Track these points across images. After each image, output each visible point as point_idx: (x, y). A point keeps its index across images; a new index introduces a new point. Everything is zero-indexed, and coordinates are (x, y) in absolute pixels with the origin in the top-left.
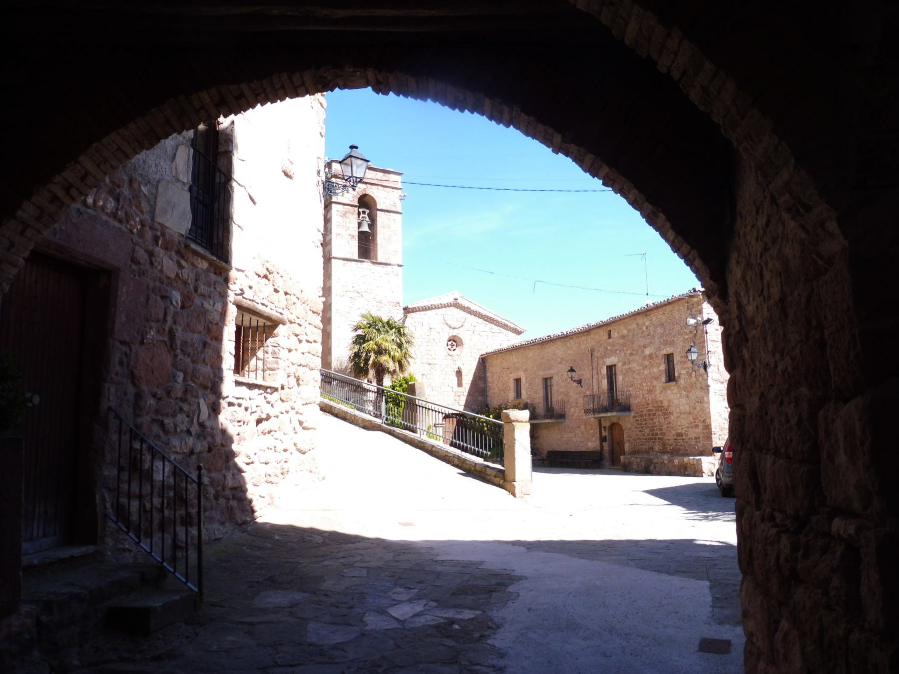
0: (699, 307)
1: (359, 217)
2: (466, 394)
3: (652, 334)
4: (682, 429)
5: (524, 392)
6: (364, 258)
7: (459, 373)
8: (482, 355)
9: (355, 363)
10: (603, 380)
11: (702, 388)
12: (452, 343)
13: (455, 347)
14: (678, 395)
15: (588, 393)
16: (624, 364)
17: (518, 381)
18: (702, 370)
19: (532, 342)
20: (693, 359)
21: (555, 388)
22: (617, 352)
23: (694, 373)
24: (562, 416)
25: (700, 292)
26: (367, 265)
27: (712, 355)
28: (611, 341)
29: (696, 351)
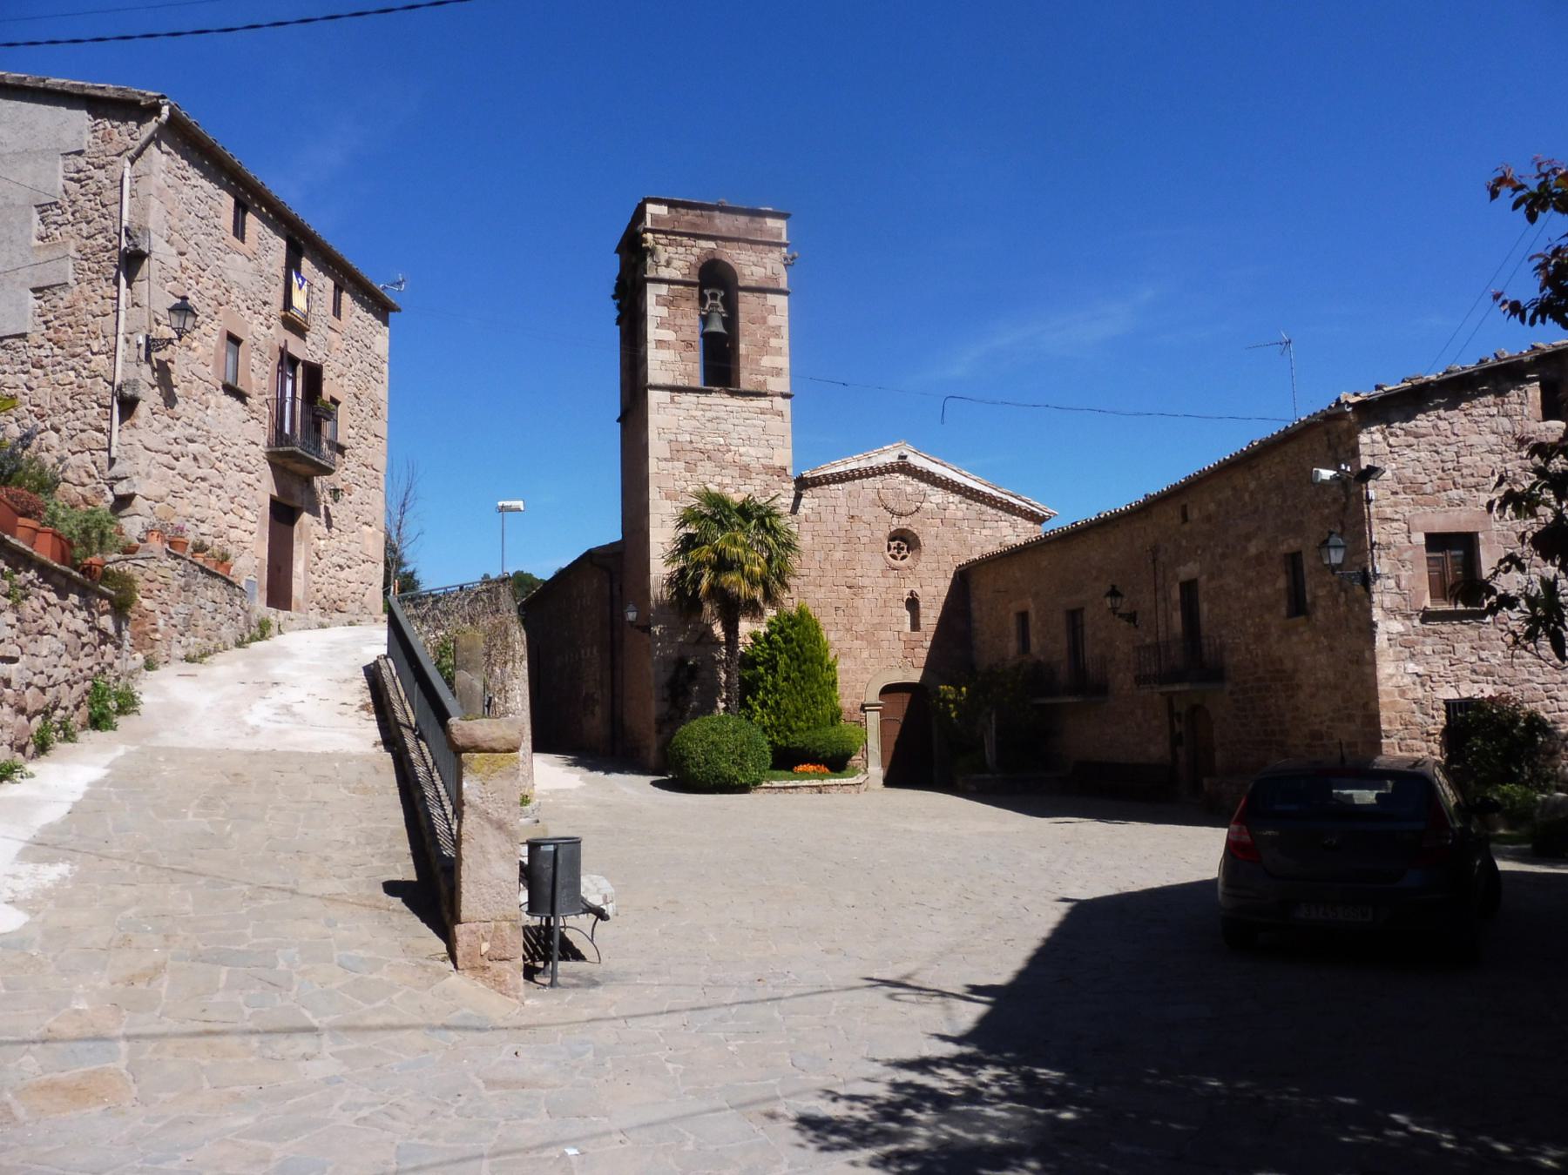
0: (1352, 442)
2: (928, 644)
3: (1261, 508)
4: (1321, 723)
5: (1033, 640)
6: (712, 385)
7: (913, 604)
9: (678, 589)
10: (1174, 614)
11: (1360, 629)
12: (899, 545)
13: (904, 552)
14: (1313, 646)
15: (1148, 640)
16: (1211, 577)
17: (1023, 617)
18: (1358, 588)
20: (1333, 562)
21: (1088, 631)
22: (1199, 552)
23: (1343, 594)
24: (1101, 689)
25: (1350, 405)
26: (719, 401)
27: (1382, 553)
28: (1187, 527)
29: (1342, 543)
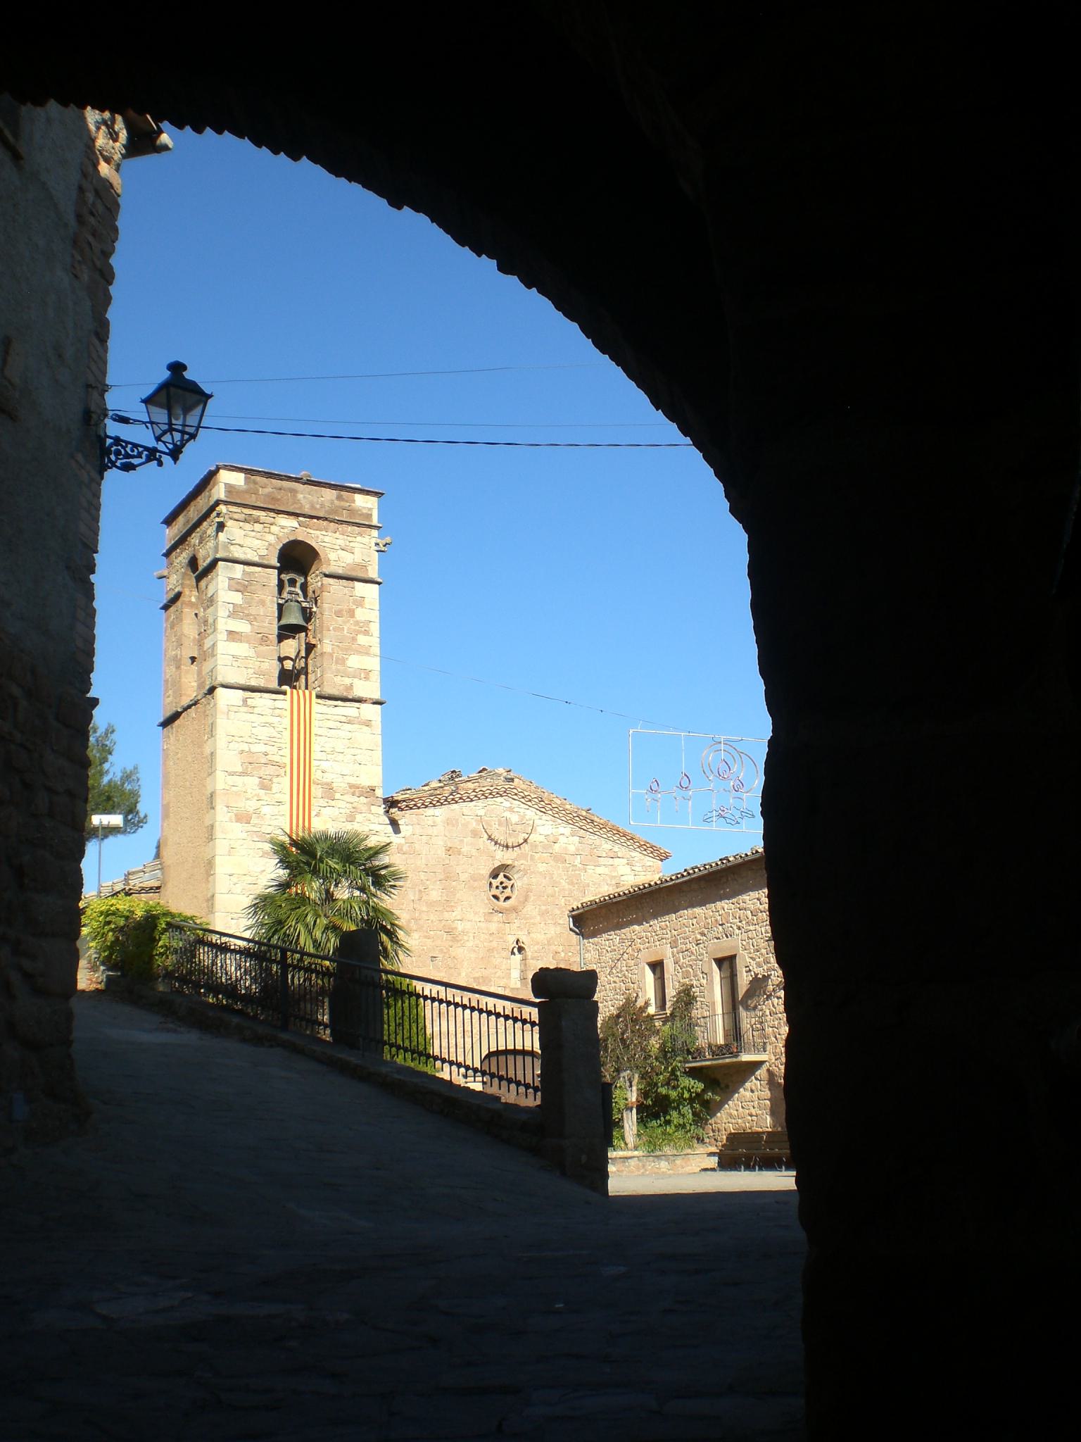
1: (280, 592)
8: (573, 910)
19: (685, 874)
